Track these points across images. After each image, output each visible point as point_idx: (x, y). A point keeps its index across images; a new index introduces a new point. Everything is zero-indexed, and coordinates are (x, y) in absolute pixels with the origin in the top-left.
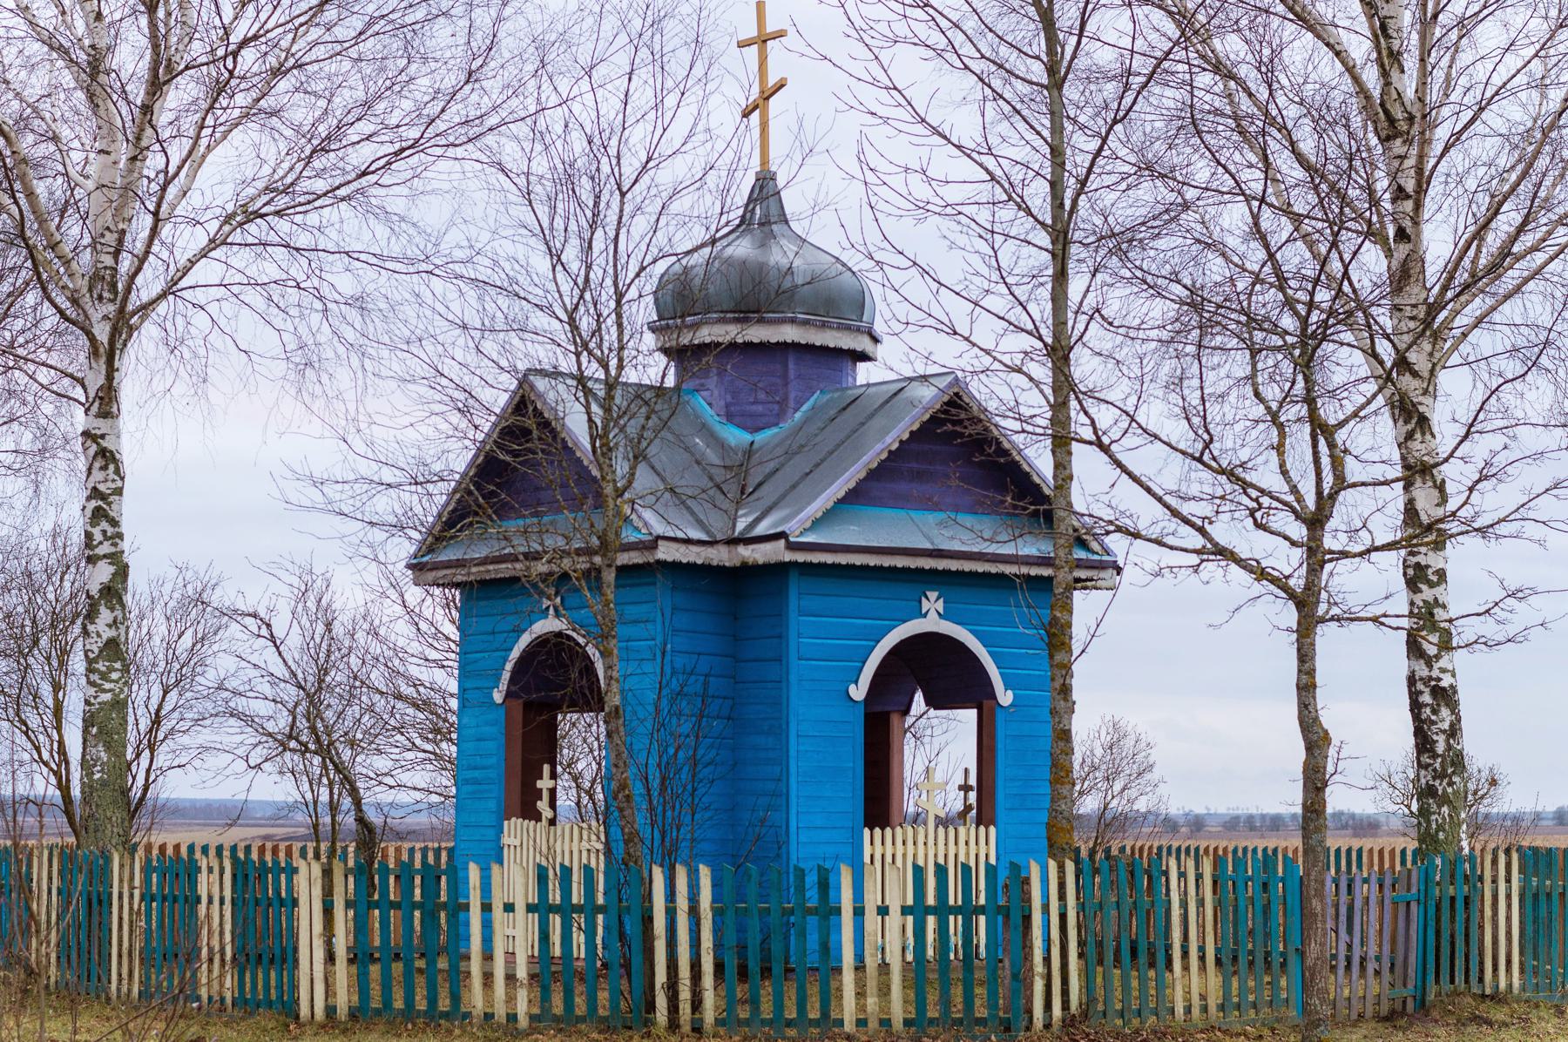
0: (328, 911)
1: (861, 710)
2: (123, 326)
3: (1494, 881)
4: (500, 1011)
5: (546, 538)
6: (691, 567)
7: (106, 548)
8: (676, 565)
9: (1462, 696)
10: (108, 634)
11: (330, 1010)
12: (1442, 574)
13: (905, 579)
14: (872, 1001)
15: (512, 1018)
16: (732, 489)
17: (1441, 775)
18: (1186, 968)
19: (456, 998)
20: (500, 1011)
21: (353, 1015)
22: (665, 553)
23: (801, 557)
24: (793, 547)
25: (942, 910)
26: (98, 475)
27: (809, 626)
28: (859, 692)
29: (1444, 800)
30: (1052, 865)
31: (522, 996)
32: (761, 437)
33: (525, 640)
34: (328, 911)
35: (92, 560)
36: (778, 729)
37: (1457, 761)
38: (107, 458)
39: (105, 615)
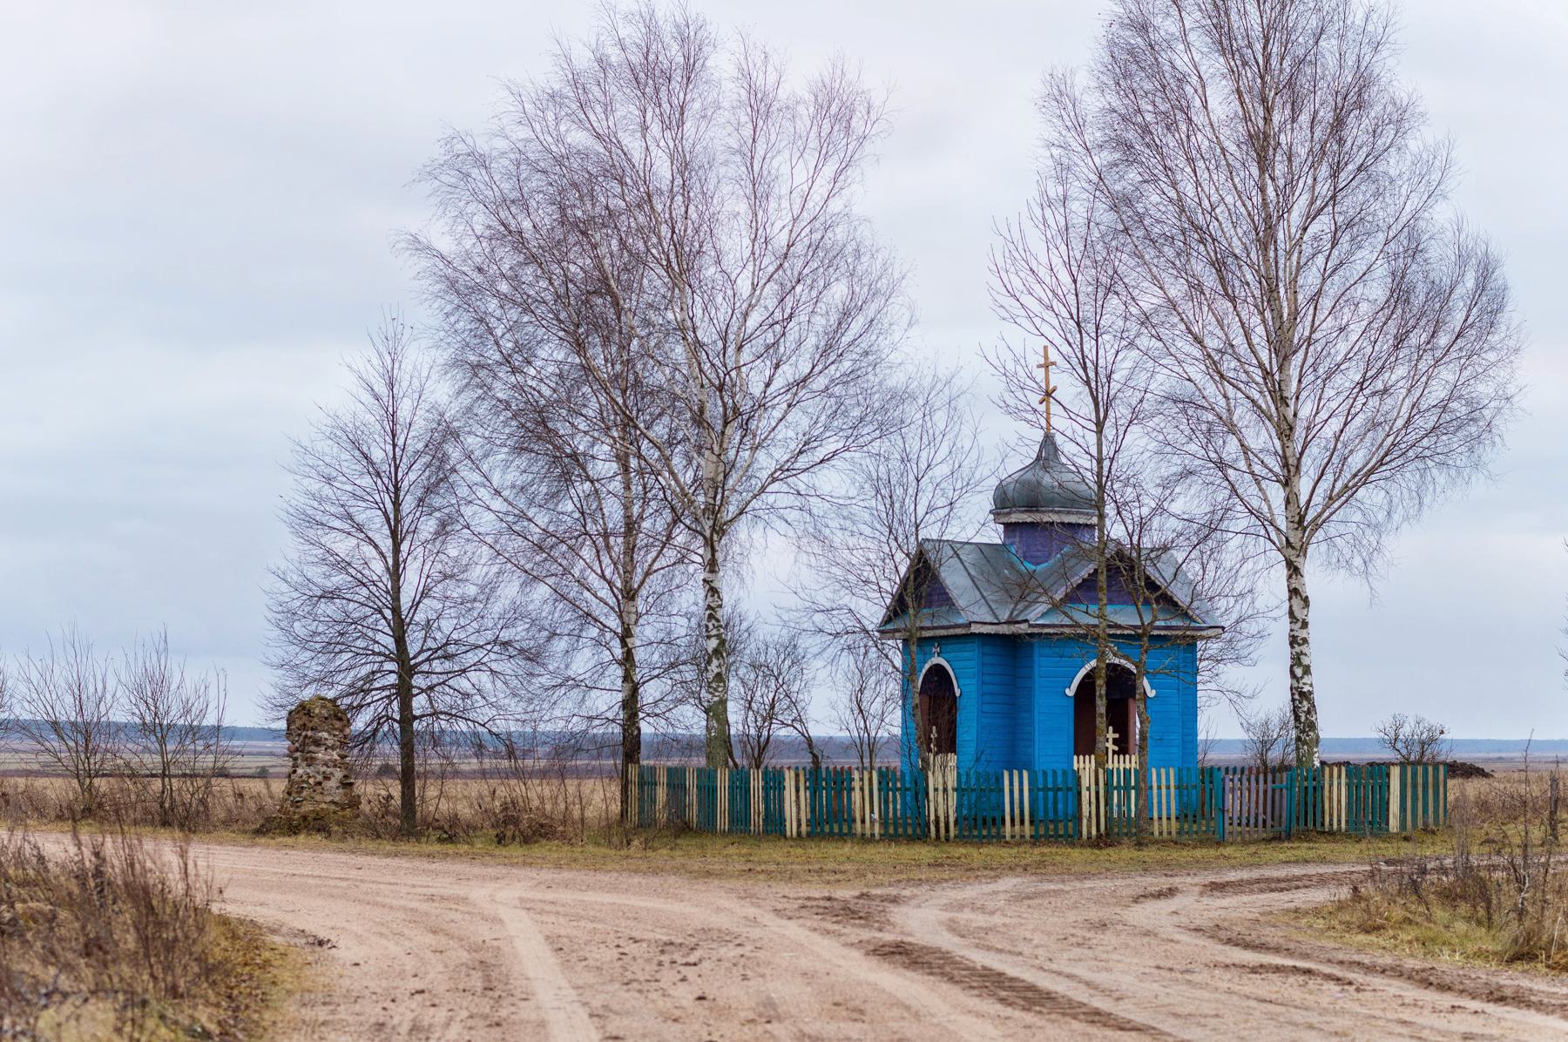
0: (797, 791)
1: (1072, 702)
2: (720, 530)
3: (1159, 788)
4: (868, 832)
5: (924, 620)
6: (988, 635)
7: (714, 632)
8: (981, 635)
9: (1317, 697)
10: (716, 670)
11: (799, 833)
12: (1305, 641)
13: (1084, 639)
14: (1017, 827)
15: (873, 835)
16: (1016, 593)
17: (1303, 732)
18: (947, 817)
19: (850, 828)
20: (868, 832)
21: (808, 835)
22: (975, 629)
23: (1036, 630)
24: (1031, 626)
25: (1046, 789)
26: (710, 599)
27: (1043, 663)
28: (1071, 692)
29: (1305, 743)
30: (1163, 771)
31: (877, 826)
32: (1040, 568)
33: (927, 666)
34: (797, 791)
35: (709, 637)
36: (1030, 710)
37: (1312, 726)
38: (713, 591)
39: (715, 662)
